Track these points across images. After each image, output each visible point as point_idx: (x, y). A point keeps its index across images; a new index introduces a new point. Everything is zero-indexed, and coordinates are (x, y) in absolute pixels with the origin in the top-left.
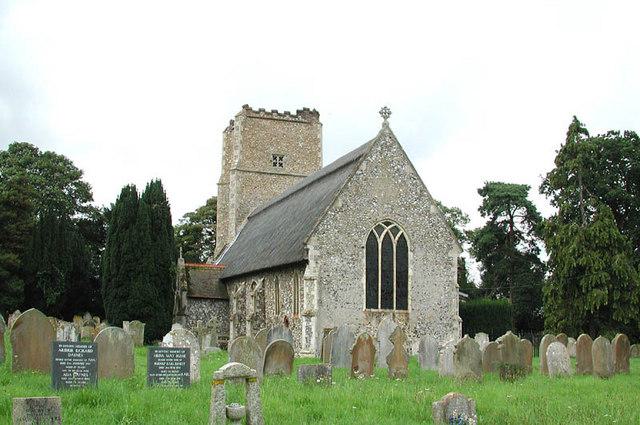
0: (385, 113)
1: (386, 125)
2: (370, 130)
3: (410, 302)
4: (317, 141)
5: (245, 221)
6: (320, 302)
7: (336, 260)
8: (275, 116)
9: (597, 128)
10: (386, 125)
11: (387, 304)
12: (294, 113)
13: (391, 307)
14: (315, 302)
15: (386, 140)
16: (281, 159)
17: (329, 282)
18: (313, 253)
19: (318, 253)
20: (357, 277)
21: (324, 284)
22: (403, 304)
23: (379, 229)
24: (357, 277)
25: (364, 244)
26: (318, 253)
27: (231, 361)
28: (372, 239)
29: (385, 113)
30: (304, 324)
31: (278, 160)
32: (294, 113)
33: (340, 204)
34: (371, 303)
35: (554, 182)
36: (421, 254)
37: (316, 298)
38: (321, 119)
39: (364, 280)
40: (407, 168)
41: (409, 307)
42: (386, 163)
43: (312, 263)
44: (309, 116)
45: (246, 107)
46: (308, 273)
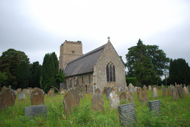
0: (109, 38)
1: (109, 41)
2: (106, 42)
3: (116, 80)
4: (81, 48)
5: (66, 65)
6: (97, 81)
7: (100, 71)
8: (69, 42)
9: (146, 43)
10: (109, 41)
11: (111, 81)
12: (76, 42)
13: (112, 81)
14: (96, 81)
15: (109, 44)
16: (74, 51)
17: (99, 76)
18: (95, 70)
19: (96, 70)
20: (104, 75)
21: (98, 77)
22: (115, 81)
23: (109, 64)
24: (104, 75)
25: (106, 67)
26: (96, 70)
27: (167, 82)
28: (107, 66)
29: (109, 38)
30: (94, 86)
31: (73, 52)
32: (76, 42)
33: (100, 58)
34: (108, 81)
35: (127, 56)
36: (118, 69)
37: (96, 80)
38: (82, 43)
39: (106, 75)
40: (114, 50)
41: (125, 80)
42: (110, 49)
43: (95, 72)
44: (79, 43)
45: (66, 41)
46: (94, 74)
